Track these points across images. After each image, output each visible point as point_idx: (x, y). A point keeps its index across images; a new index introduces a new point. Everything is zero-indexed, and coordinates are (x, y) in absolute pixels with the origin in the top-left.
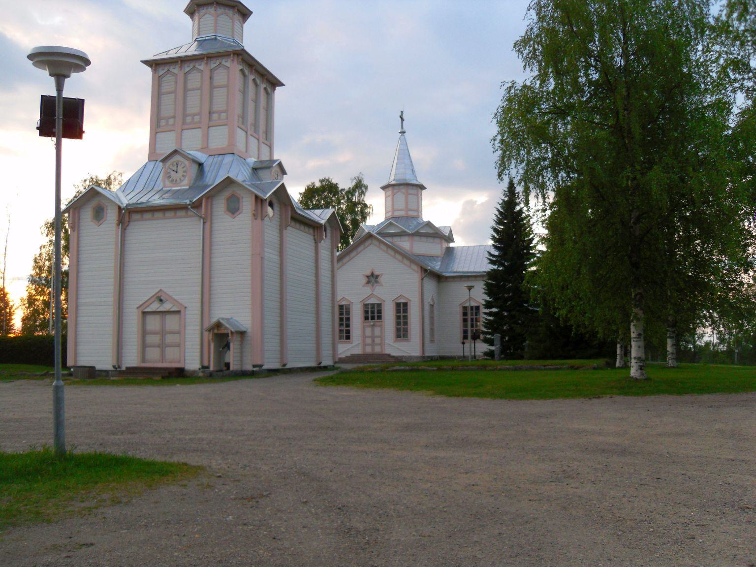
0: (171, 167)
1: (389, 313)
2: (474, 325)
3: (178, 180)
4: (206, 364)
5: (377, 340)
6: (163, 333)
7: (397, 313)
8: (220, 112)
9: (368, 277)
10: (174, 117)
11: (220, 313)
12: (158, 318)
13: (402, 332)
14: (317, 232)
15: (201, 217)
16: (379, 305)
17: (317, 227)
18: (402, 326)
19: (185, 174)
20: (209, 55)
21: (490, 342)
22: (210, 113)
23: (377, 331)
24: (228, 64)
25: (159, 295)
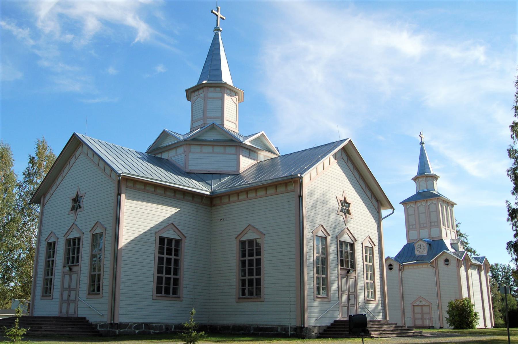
2: (247, 291)
6: (422, 313)
8: (434, 222)
10: (415, 225)
12: (420, 307)
15: (434, 267)
19: (424, 249)
22: (430, 223)
24: (413, 206)
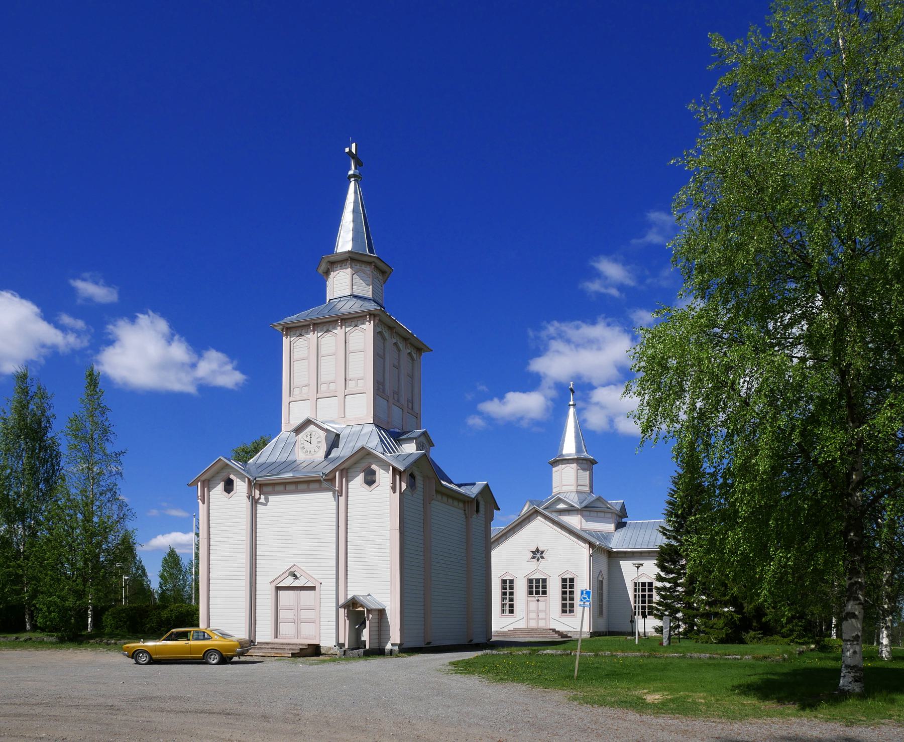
0: (305, 437)
1: (554, 589)
3: (312, 451)
4: (341, 641)
5: (542, 615)
6: (298, 608)
7: (563, 588)
9: (533, 552)
11: (355, 590)
13: (567, 608)
14: (468, 506)
16: (544, 581)
17: (468, 502)
18: (568, 602)
19: (319, 445)
20: (343, 317)
21: (660, 617)
23: (542, 605)
25: (292, 570)
